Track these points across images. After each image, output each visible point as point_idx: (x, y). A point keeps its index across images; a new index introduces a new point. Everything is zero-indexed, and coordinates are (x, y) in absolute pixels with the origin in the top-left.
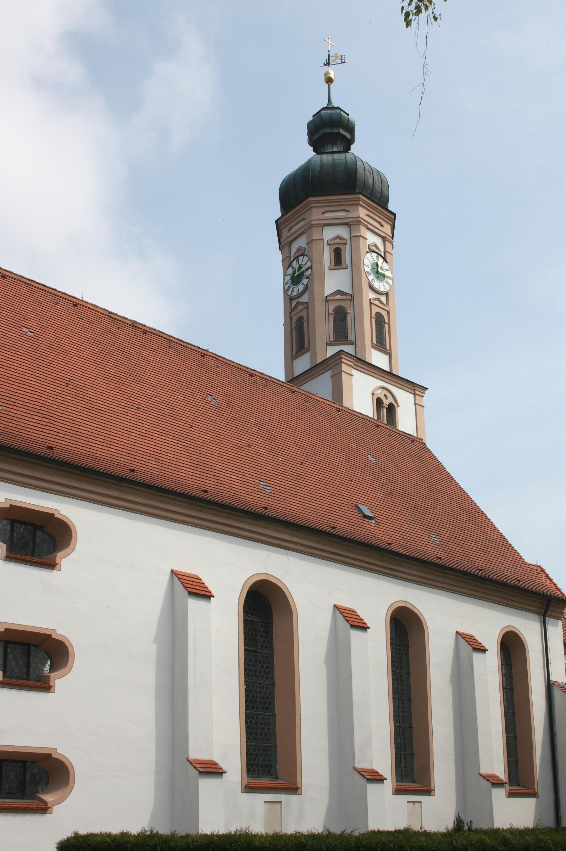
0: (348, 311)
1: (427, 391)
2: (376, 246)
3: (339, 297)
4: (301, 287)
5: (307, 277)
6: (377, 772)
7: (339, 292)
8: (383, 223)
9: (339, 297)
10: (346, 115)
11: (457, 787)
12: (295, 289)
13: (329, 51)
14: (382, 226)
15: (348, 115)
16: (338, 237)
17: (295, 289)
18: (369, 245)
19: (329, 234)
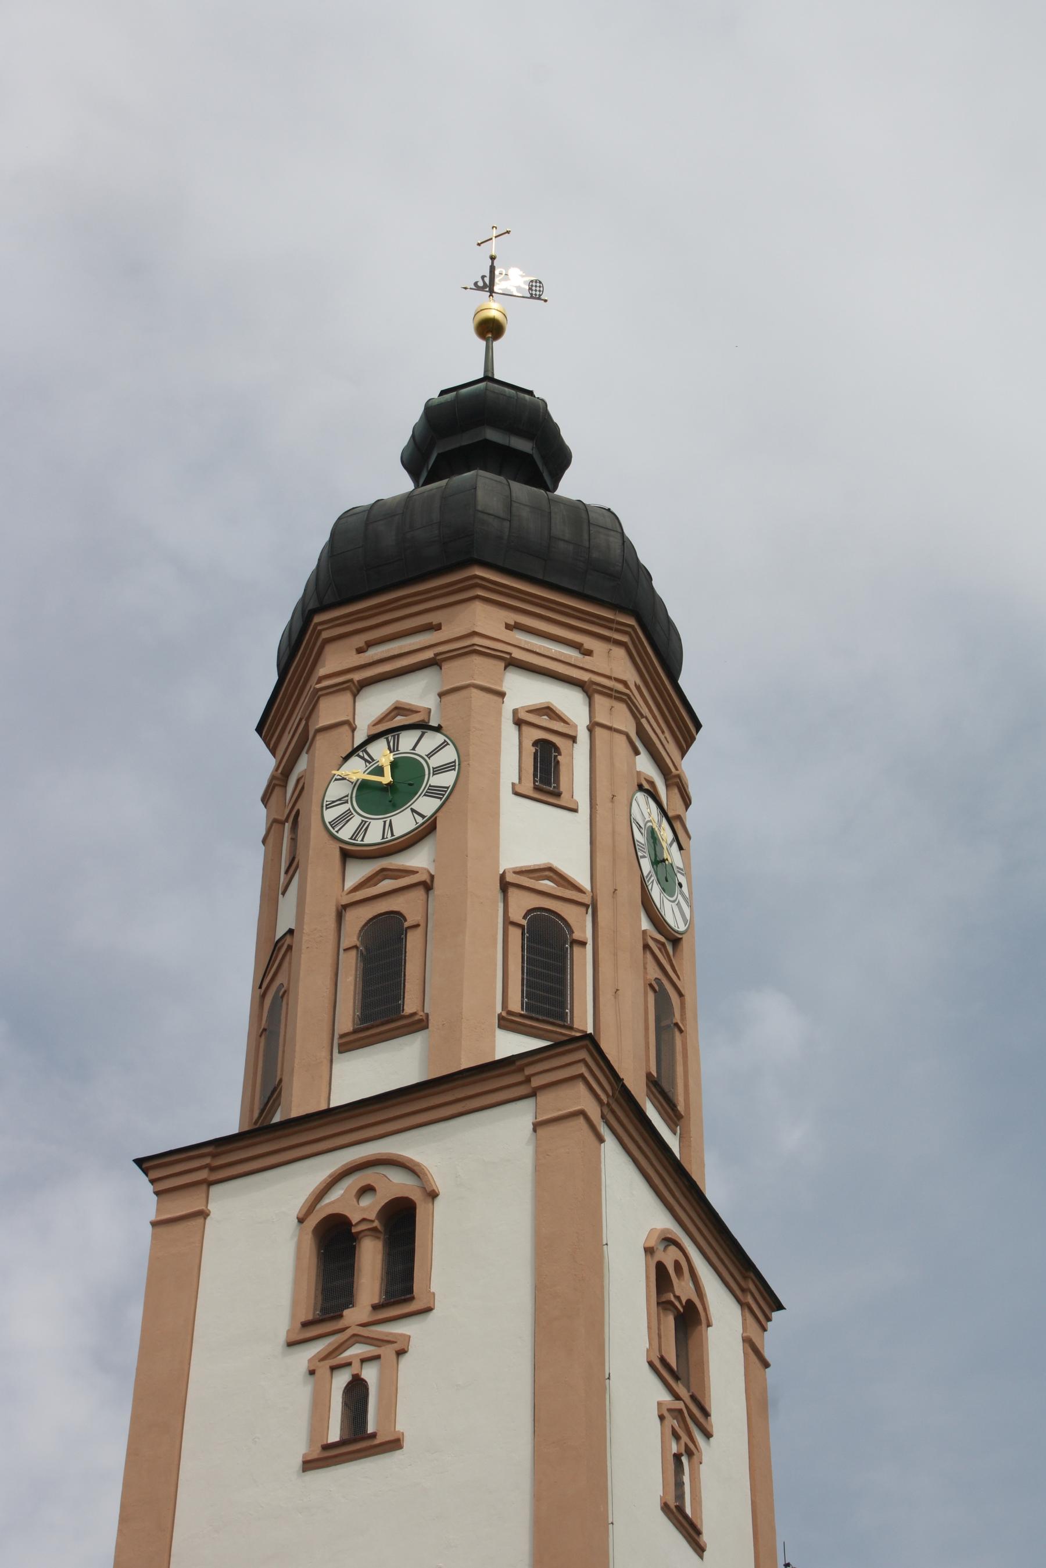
0: (577, 935)
1: (776, 1315)
2: (652, 783)
3: (546, 885)
4: (403, 823)
5: (434, 792)
6: (706, 1414)
7: (550, 872)
8: (588, 642)
9: (546, 885)
10: (527, 397)
11: (652, 761)
12: (356, 821)
13: (493, 258)
14: (588, 653)
15: (531, 393)
16: (547, 710)
17: (356, 821)
18: (515, 712)
19: (524, 692)
